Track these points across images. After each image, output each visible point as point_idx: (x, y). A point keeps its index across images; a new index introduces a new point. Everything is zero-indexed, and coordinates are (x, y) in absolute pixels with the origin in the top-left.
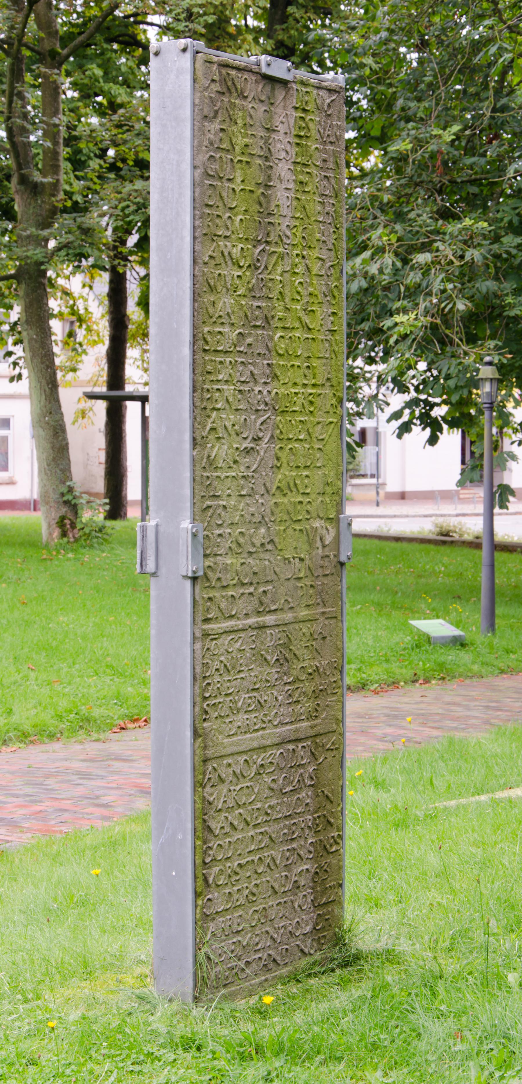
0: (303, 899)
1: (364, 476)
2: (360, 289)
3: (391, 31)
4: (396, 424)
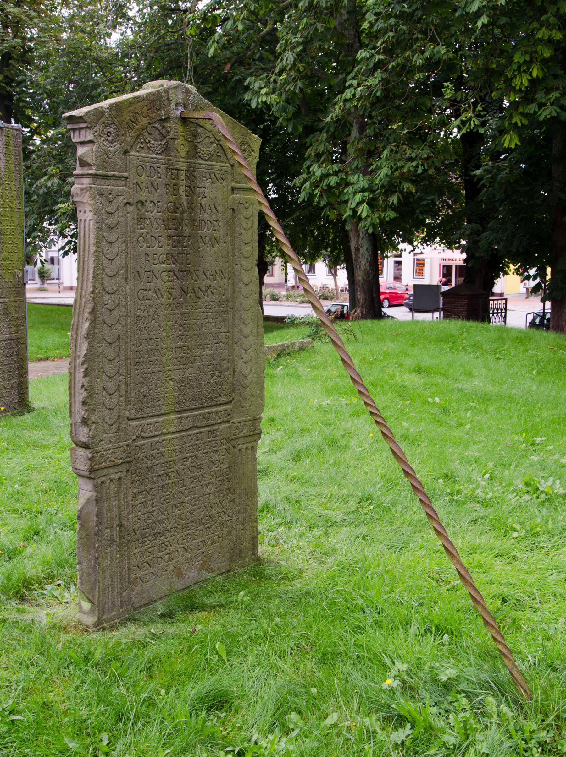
0: (15, 391)
1: (53, 279)
2: (44, 193)
3: (56, 78)
4: (62, 252)
